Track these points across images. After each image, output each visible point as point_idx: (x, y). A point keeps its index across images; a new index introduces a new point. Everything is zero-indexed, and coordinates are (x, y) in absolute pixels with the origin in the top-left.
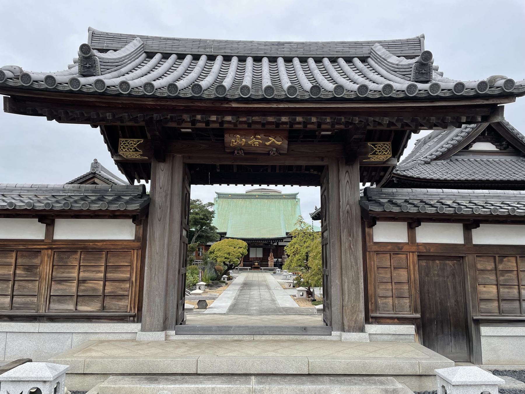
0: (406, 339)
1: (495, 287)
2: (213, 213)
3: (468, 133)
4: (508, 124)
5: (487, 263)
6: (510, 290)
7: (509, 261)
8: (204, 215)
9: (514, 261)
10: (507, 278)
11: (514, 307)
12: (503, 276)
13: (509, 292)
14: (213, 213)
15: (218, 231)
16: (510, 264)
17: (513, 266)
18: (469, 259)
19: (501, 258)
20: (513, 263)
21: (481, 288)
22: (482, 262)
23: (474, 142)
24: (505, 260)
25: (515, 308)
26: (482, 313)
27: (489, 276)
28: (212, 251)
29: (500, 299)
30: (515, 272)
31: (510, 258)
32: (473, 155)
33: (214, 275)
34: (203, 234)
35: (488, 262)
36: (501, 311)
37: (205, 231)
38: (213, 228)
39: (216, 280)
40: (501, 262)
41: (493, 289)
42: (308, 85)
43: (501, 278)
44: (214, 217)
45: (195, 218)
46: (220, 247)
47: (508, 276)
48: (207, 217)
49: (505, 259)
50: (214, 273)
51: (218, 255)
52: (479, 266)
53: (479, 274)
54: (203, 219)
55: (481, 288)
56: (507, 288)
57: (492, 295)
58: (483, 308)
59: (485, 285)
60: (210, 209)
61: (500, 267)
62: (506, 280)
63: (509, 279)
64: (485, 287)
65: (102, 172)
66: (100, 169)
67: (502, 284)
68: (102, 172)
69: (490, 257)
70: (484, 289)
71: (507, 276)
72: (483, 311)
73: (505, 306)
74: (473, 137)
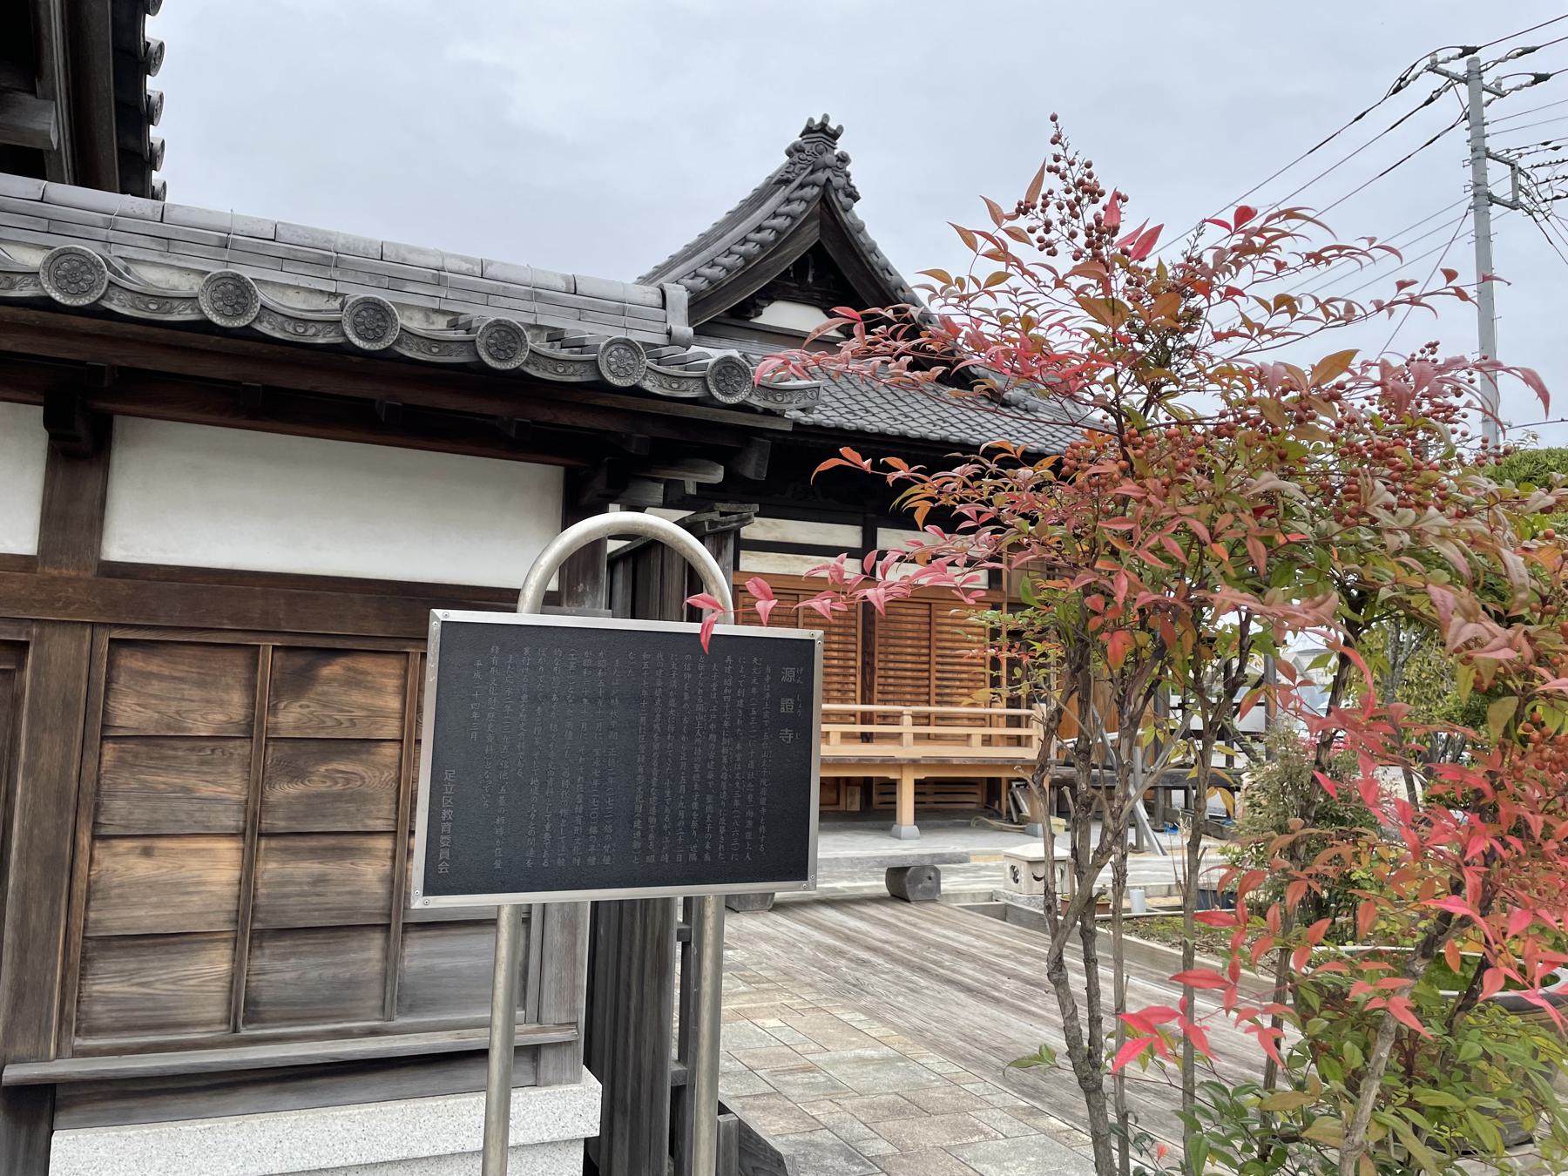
1: (228, 852)
3: (747, 258)
4: (873, 249)
5: (197, 693)
6: (332, 868)
7: (355, 681)
9: (392, 684)
10: (322, 788)
11: (344, 973)
12: (298, 775)
13: (321, 880)
16: (357, 697)
17: (375, 714)
18: (60, 656)
19: (299, 661)
20: (380, 691)
21: (121, 865)
22: (155, 687)
23: (771, 294)
24: (327, 671)
25: (351, 983)
26: (91, 1031)
27: (191, 781)
29: (253, 927)
30: (389, 752)
31: (365, 663)
32: (761, 340)
35: (201, 684)
36: (245, 1010)
40: (297, 683)
41: (214, 869)
42: (704, 286)
43: (284, 791)
47: (328, 776)
49: (333, 670)
52: (129, 712)
53: (121, 762)
55: (121, 865)
56: (314, 853)
57: (196, 902)
58: (107, 999)
59: (148, 837)
61: (290, 717)
62: (315, 804)
63: (338, 797)
64: (147, 853)
67: (281, 825)
69: (229, 655)
70: (142, 868)
71: (321, 779)
72: (105, 1020)
73: (282, 971)
74: (762, 276)
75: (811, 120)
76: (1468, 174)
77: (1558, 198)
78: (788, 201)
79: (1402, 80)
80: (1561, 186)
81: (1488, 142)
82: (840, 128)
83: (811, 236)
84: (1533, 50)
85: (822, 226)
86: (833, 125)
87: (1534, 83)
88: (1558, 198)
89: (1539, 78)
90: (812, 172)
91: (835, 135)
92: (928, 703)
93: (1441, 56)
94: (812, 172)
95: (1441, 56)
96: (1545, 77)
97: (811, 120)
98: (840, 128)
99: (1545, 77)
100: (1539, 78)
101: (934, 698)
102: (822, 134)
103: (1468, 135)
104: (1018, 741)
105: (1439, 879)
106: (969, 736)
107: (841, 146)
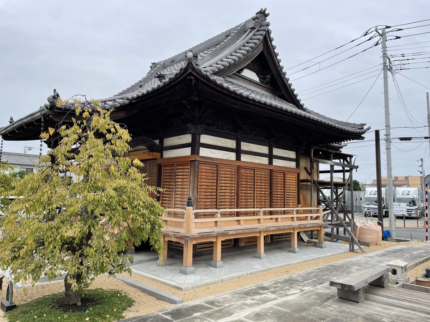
42: (237, 59)
74: (249, 59)
75: (262, 9)
76: (382, 61)
77: (402, 69)
78: (255, 35)
79: (367, 33)
80: (403, 66)
81: (387, 52)
82: (269, 13)
83: (261, 49)
84: (402, 30)
85: (264, 45)
86: (267, 12)
87: (396, 39)
88: (402, 69)
89: (397, 38)
90: (260, 27)
91: (267, 15)
92: (254, 208)
93: (378, 28)
94: (260, 27)
95: (378, 28)
96: (399, 38)
97: (262, 9)
98: (269, 13)
99: (399, 38)
100: (397, 38)
101: (255, 206)
102: (263, 14)
103: (382, 50)
104: (317, 218)
105: (92, 243)
106: (306, 217)
107: (268, 19)
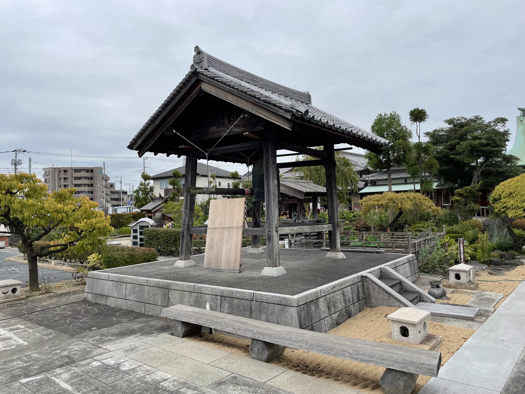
0: (123, 233)
2: (506, 133)
8: (488, 139)
14: (506, 133)
15: (520, 163)
28: (497, 197)
33: (509, 240)
34: (491, 169)
37: (496, 165)
38: (509, 159)
39: (511, 248)
44: (508, 140)
45: (471, 146)
46: (511, 190)
48: (494, 141)
50: (509, 236)
51: (509, 205)
54: (487, 145)
60: (500, 128)
65: (211, 69)
66: (205, 64)
68: (211, 69)
